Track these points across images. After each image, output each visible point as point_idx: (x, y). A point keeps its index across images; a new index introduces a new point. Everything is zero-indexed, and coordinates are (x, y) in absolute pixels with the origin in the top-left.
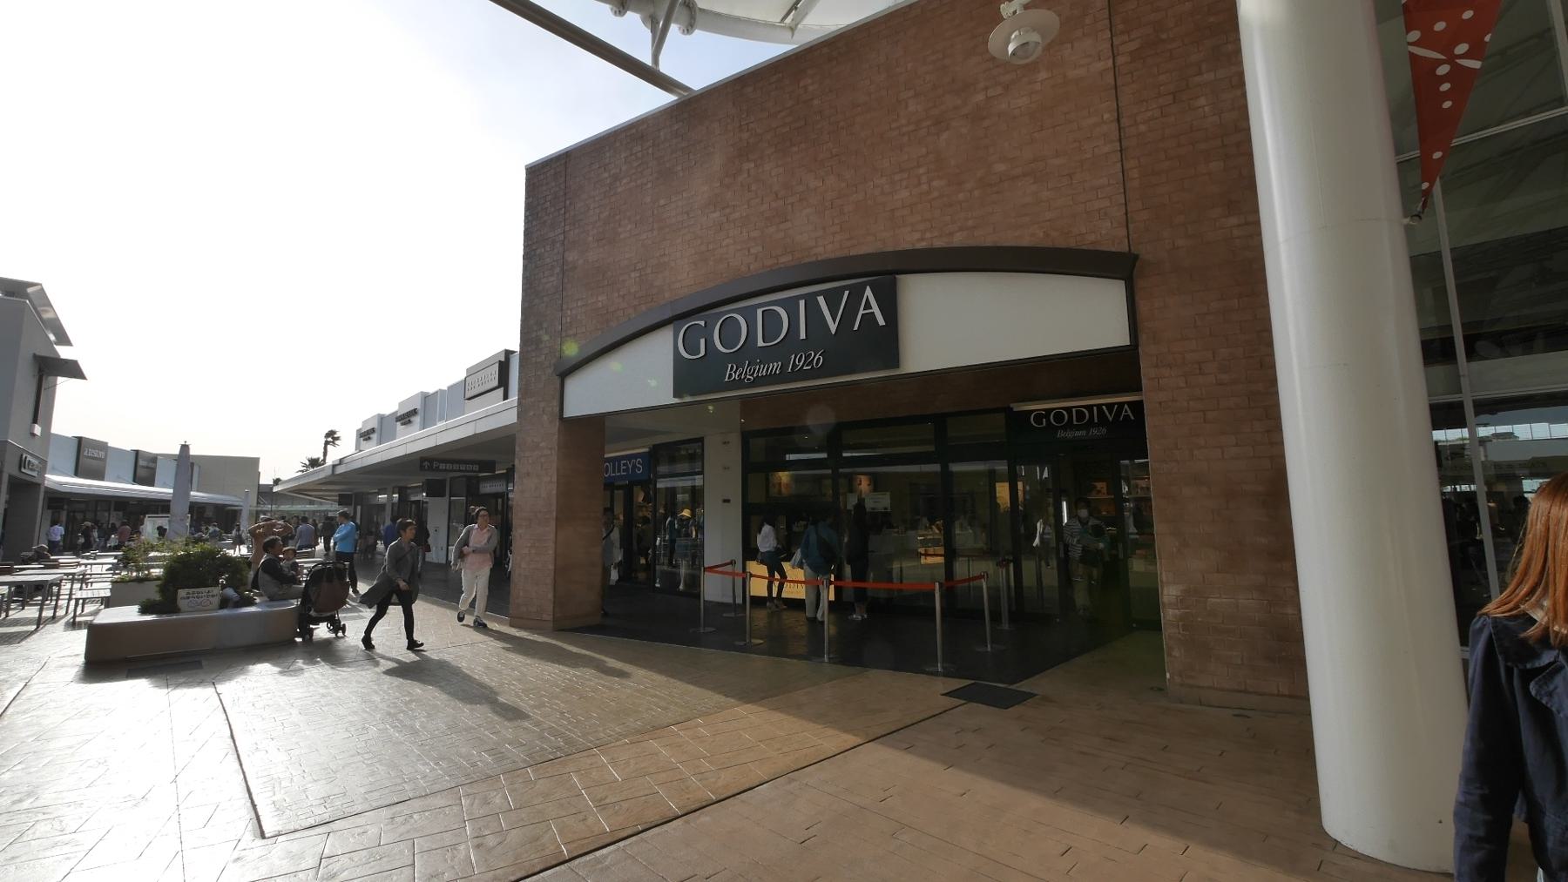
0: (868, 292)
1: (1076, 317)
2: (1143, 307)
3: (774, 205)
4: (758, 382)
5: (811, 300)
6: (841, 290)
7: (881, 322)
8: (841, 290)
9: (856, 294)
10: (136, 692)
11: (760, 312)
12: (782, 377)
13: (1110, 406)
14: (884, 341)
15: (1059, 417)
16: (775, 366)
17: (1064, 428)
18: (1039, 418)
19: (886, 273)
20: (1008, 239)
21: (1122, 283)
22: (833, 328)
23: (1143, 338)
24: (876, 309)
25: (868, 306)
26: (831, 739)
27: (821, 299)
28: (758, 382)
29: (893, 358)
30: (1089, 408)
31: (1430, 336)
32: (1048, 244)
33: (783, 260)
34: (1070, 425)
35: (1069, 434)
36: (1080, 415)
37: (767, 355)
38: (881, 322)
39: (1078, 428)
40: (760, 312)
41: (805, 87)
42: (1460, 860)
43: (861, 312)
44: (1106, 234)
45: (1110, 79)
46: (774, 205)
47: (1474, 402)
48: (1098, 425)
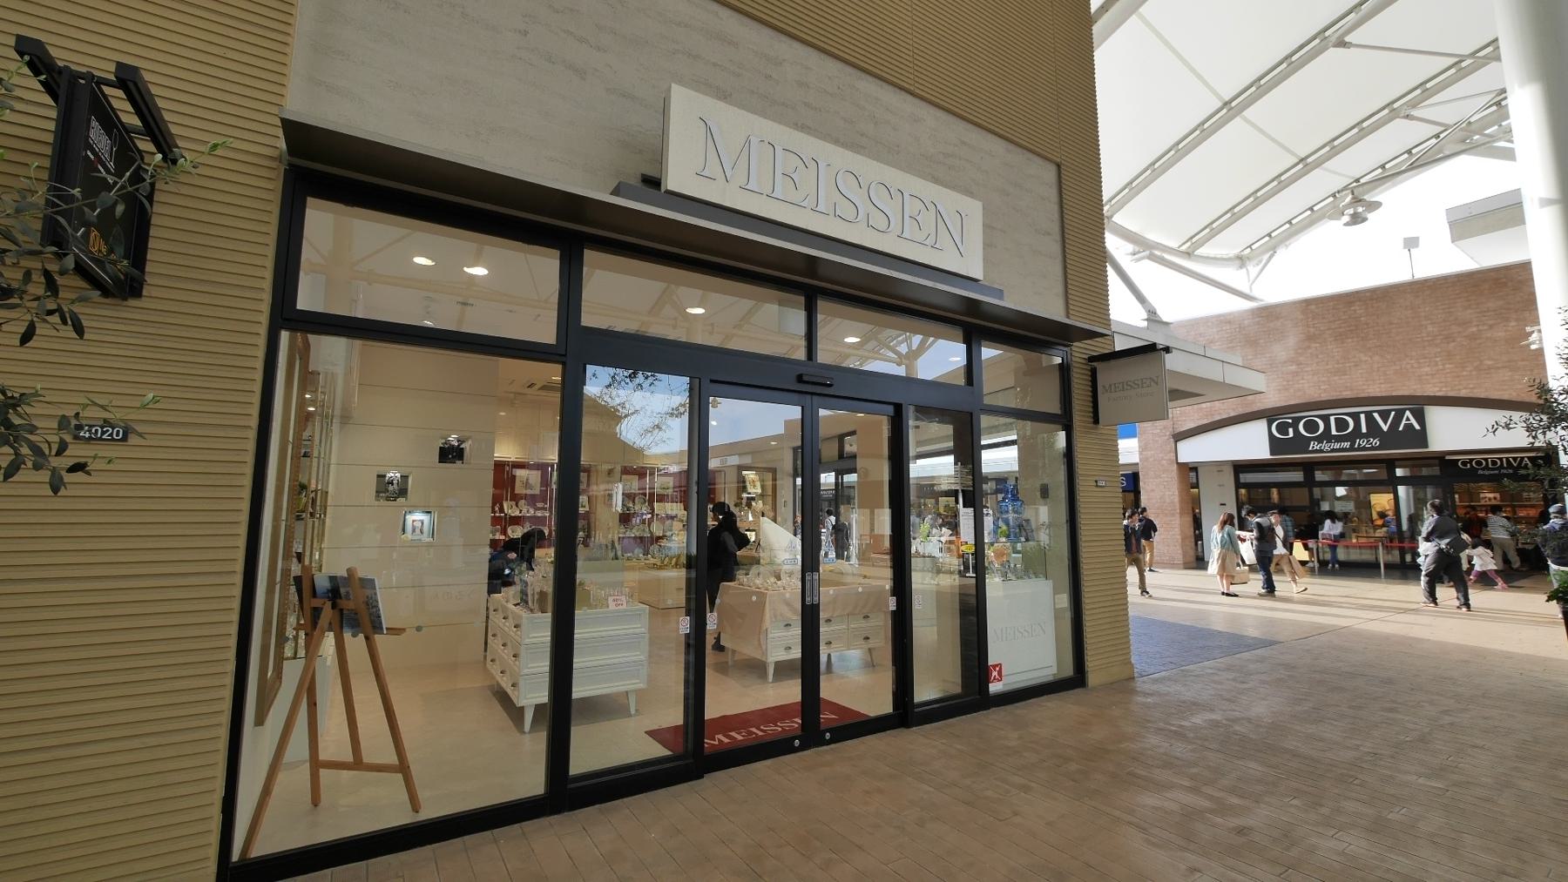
0: (1408, 413)
4: (1333, 450)
5: (1369, 415)
6: (1389, 411)
8: (1389, 411)
10: (490, 476)
15: (1479, 463)
17: (1319, 439)
18: (1464, 463)
19: (1419, 405)
20: (1506, 396)
21: (557, 253)
24: (1413, 421)
26: (406, 231)
28: (1333, 450)
31: (1527, 314)
34: (1327, 436)
35: (1325, 446)
36: (1494, 463)
39: (1339, 439)
47: (1526, 267)
48: (1366, 436)
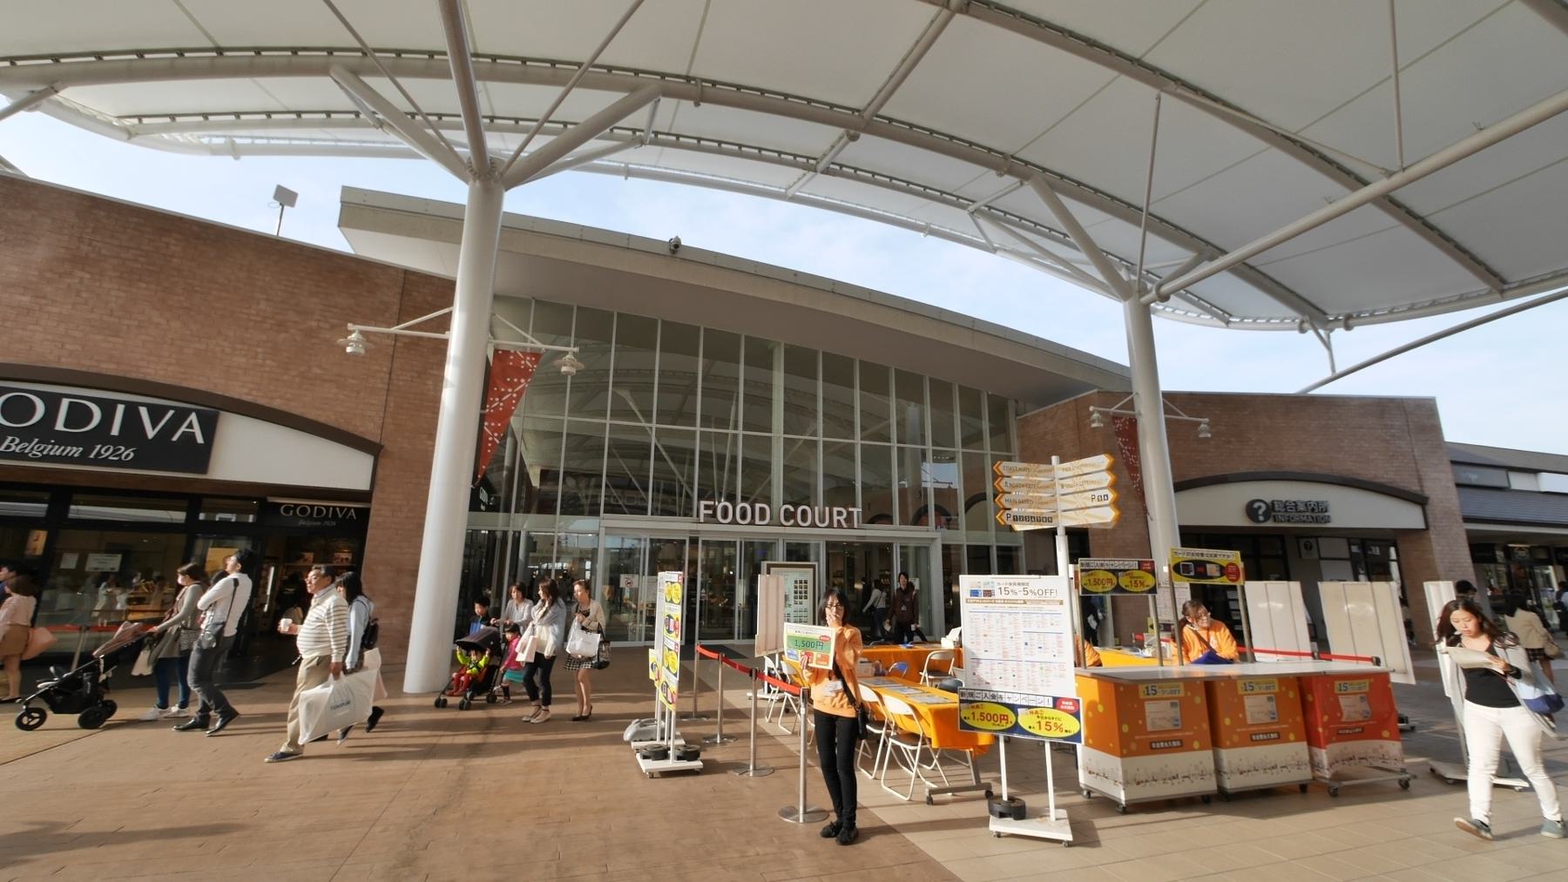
0: (193, 417)
1: (346, 470)
2: (379, 471)
3: (106, 318)
5: (132, 409)
6: (166, 409)
7: (200, 440)
8: (166, 409)
9: (181, 415)
11: (65, 403)
12: (83, 459)
13: (342, 509)
14: (199, 455)
15: (303, 510)
16: (76, 451)
17: (26, 435)
18: (287, 509)
19: (212, 409)
20: (312, 414)
22: (151, 433)
23: (377, 489)
25: (190, 426)
27: (143, 411)
29: (204, 468)
30: (327, 508)
32: (336, 425)
33: (105, 366)
37: (63, 439)
38: (200, 440)
39: (63, 439)
40: (65, 403)
41: (167, 244)
42: (466, 182)
43: (183, 429)
44: (370, 431)
45: (390, 350)
46: (106, 318)
